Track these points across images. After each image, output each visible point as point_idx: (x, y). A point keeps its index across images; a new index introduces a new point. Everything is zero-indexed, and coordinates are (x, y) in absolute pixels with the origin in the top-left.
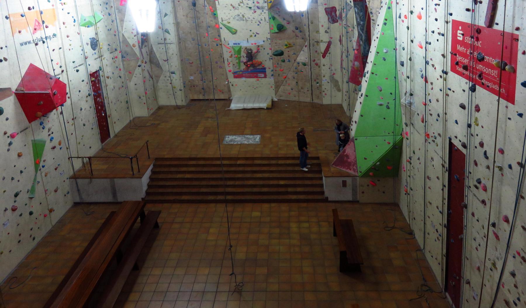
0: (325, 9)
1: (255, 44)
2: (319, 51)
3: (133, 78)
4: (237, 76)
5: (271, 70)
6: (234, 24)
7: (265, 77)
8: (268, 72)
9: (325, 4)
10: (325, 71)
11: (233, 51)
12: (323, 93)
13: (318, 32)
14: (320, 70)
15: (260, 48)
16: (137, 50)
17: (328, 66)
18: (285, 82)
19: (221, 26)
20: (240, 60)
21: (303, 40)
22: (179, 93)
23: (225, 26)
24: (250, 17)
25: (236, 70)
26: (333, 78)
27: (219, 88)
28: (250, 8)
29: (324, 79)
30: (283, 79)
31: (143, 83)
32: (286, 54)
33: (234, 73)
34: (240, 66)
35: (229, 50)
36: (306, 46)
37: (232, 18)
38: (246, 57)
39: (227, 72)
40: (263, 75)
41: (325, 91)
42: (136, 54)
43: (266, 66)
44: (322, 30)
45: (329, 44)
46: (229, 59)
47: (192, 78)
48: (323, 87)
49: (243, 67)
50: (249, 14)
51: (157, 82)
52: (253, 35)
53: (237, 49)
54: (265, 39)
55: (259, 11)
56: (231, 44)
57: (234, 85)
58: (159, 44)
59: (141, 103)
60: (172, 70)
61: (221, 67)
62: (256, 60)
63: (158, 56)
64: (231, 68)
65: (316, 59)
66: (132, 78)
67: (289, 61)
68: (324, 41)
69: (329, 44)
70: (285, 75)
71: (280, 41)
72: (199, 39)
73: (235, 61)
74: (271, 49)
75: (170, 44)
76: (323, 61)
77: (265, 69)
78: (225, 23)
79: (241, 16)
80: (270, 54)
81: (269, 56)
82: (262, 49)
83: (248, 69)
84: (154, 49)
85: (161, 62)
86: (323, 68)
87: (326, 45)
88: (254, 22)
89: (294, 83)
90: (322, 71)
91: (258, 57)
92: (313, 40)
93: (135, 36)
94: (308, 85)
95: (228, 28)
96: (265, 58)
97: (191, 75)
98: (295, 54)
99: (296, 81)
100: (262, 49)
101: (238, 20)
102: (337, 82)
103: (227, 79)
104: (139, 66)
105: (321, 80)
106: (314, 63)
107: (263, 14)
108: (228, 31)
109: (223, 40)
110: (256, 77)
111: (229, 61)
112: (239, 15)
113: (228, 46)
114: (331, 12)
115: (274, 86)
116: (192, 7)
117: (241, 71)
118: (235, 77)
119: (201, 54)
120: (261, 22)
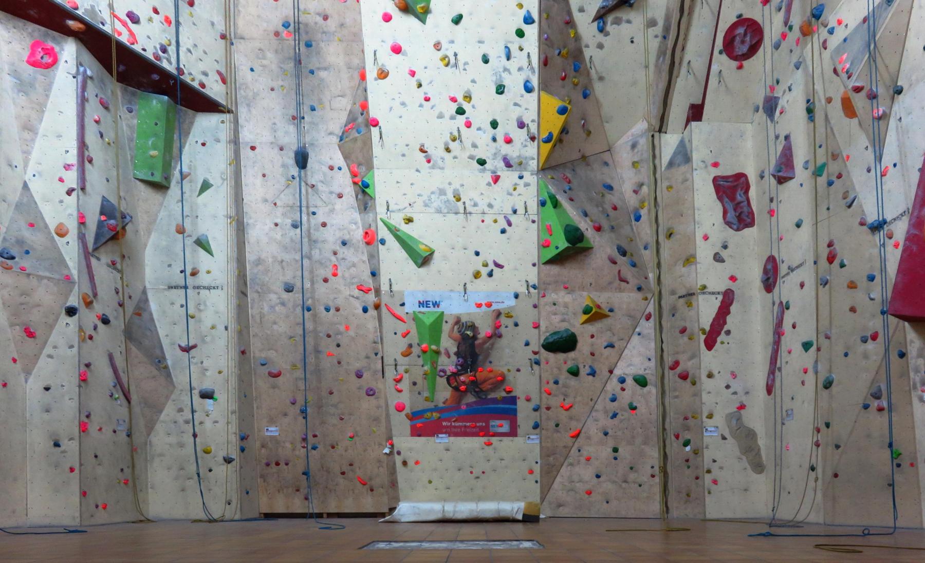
0: (715, 180)
1: (489, 305)
2: (693, 327)
3: (43, 361)
4: (424, 426)
5: (532, 405)
6: (423, 232)
7: (513, 433)
8: (524, 410)
9: (716, 165)
10: (714, 397)
11: (414, 331)
12: (708, 478)
13: (690, 260)
14: (697, 395)
15: (503, 320)
16: (70, 250)
17: (726, 378)
18: (574, 451)
19: (383, 233)
20: (434, 364)
21: (639, 295)
22: (222, 471)
23: (394, 231)
24: (477, 199)
25: (421, 405)
26: (739, 419)
27: (359, 473)
28: (482, 162)
29: (708, 423)
30: (570, 441)
31: (75, 380)
32: (584, 345)
33: (413, 417)
34: (433, 389)
35: (401, 328)
36: (648, 318)
37: (419, 205)
38: (457, 354)
39: (392, 410)
40: (506, 428)
41: (715, 468)
42: (62, 262)
43: (519, 392)
44: (704, 252)
45: (728, 299)
46: (402, 360)
47: (273, 431)
48: (708, 455)
49: (444, 393)
50: (475, 185)
51: (150, 428)
52: (484, 271)
53: (428, 320)
54: (522, 290)
55: (509, 177)
56: (411, 307)
57: (411, 463)
58: (170, 287)
59: (56, 466)
60: (207, 385)
61: (371, 393)
62: (488, 367)
63: (162, 333)
64: (405, 398)
65: (682, 358)
66: (37, 357)
67: (593, 373)
68: (710, 289)
69: (728, 299)
70: (575, 426)
71: (568, 298)
72: (307, 285)
73: (419, 368)
74: (536, 326)
75: (209, 288)
76: (709, 359)
77: (513, 400)
78: (397, 220)
79: (450, 196)
80: (535, 345)
81: (528, 353)
82: (510, 322)
83: (459, 401)
84: (153, 306)
85: (172, 355)
86: (707, 384)
87: (717, 304)
88: (489, 219)
89: (607, 451)
90: (705, 396)
91: (494, 356)
92: (673, 293)
93: (69, 192)
94: (653, 455)
95: (406, 244)
96: (516, 362)
97: (272, 421)
98: (611, 346)
99: (611, 443)
100: (510, 322)
101: (439, 211)
102: (751, 435)
103: (390, 439)
104: (71, 312)
105: (702, 428)
106: (674, 372)
107: (521, 189)
108: (403, 254)
109: (384, 288)
110: (485, 432)
111: (401, 369)
112: (442, 192)
113: (400, 311)
114: (734, 190)
115: (537, 469)
116: (295, 171)
117: (436, 409)
118: (416, 432)
119: (310, 341)
120: (513, 218)
